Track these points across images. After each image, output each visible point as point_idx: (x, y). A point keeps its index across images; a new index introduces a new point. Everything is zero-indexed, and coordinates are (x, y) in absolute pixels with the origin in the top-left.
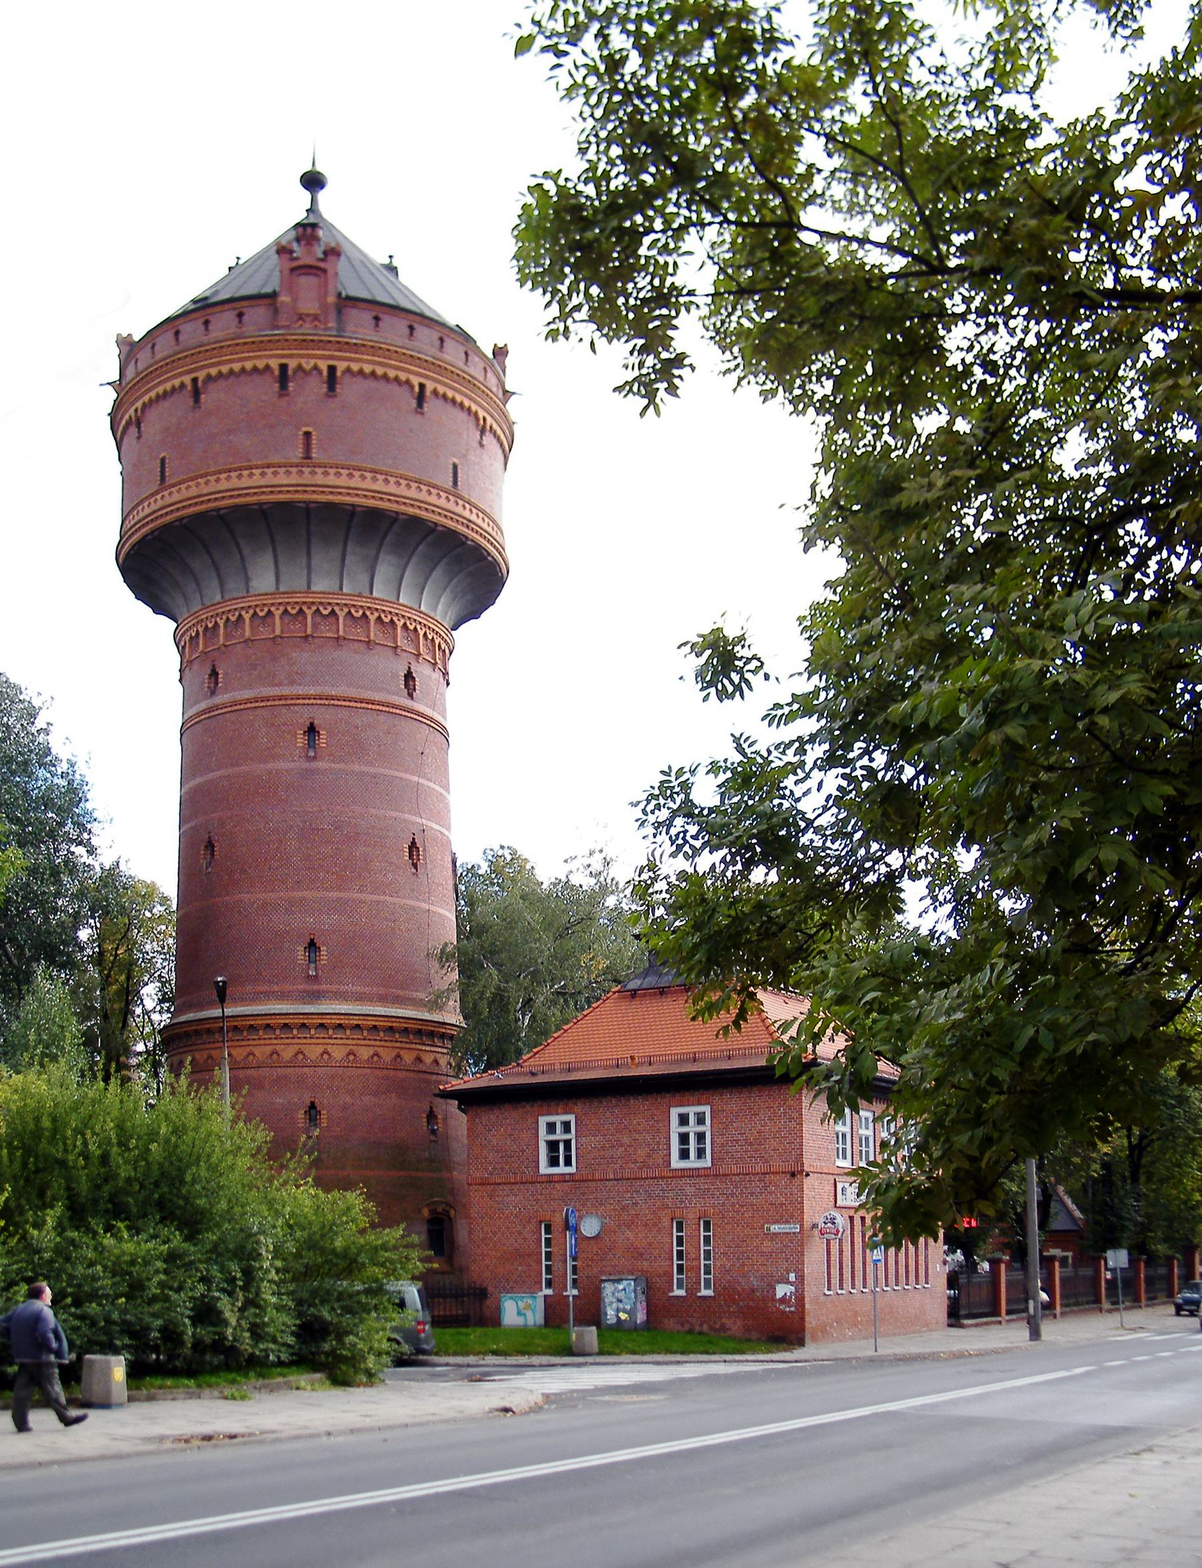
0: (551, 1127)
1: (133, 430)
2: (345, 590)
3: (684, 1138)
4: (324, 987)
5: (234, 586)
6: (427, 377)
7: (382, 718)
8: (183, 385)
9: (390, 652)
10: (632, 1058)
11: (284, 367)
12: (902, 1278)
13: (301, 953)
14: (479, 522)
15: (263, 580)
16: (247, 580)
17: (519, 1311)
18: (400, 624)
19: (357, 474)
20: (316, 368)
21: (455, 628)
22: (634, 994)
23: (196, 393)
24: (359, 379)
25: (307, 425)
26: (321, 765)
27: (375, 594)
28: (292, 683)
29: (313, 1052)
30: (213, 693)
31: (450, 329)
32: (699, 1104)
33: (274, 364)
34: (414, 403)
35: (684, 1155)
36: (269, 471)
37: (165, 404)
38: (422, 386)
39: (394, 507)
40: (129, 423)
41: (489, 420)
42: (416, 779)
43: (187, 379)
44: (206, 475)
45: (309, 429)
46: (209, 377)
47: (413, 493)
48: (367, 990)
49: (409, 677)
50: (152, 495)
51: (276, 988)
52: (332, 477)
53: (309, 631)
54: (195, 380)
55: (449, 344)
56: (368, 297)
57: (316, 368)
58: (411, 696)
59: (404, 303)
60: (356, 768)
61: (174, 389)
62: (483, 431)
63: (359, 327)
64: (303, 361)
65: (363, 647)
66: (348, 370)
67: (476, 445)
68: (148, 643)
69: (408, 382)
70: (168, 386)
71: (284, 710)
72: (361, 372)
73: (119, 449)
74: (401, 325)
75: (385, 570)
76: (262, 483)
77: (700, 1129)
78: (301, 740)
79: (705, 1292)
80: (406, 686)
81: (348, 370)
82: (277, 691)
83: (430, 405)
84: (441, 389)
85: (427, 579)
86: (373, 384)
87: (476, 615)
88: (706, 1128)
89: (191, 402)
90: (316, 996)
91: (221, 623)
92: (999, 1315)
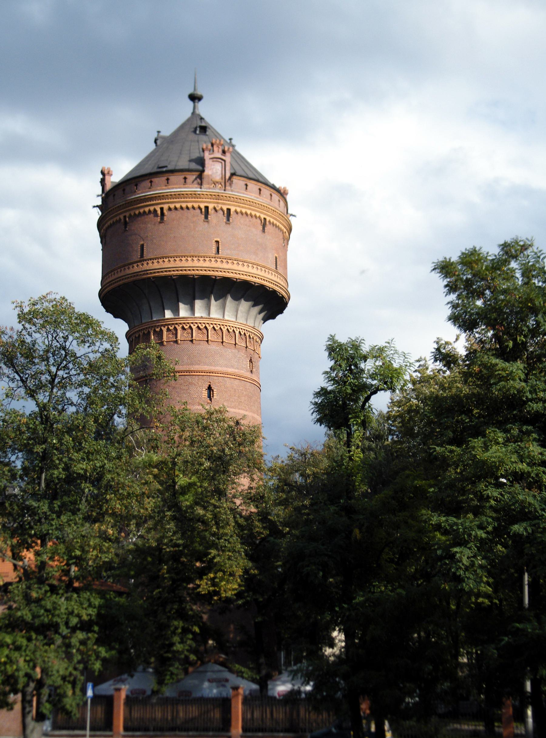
20: (222, 209)
25: (217, 237)
41: (268, 219)
43: (122, 217)
45: (218, 240)
54: (125, 217)
59: (261, 179)
61: (117, 221)
81: (236, 212)
84: (239, 210)
85: (237, 311)
87: (273, 317)
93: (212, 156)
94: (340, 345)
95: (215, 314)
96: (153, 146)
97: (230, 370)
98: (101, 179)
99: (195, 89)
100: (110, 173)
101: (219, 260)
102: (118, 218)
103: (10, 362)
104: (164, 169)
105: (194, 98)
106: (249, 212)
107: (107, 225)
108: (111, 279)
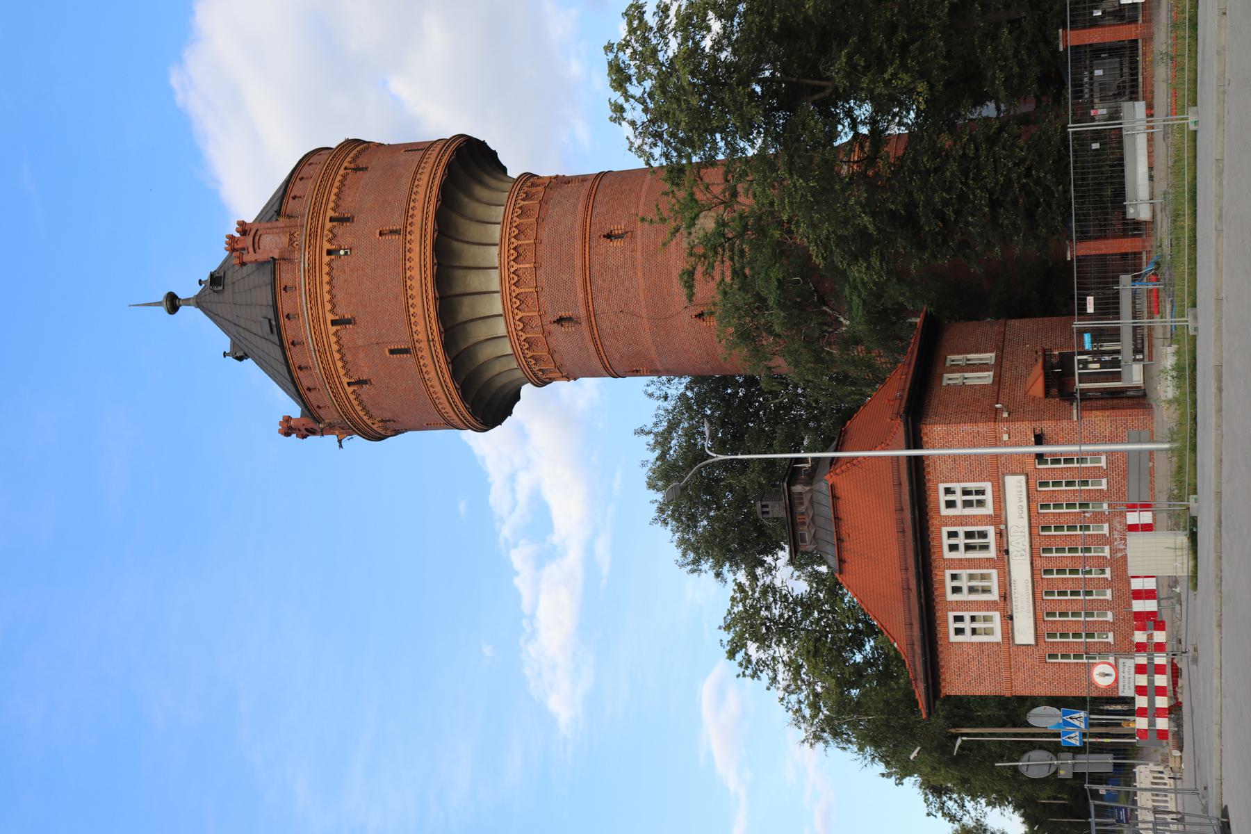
11: (334, 323)
19: (412, 310)
22: (841, 561)
23: (360, 382)
32: (937, 491)
43: (350, 390)
52: (419, 328)
57: (331, 231)
66: (332, 311)
73: (406, 430)
77: (962, 535)
81: (332, 311)
88: (957, 487)
93: (251, 249)
95: (500, 328)
96: (249, 362)
97: (579, 282)
99: (159, 304)
100: (288, 419)
101: (409, 228)
102: (352, 397)
104: (274, 323)
105: (173, 303)
108: (452, 413)
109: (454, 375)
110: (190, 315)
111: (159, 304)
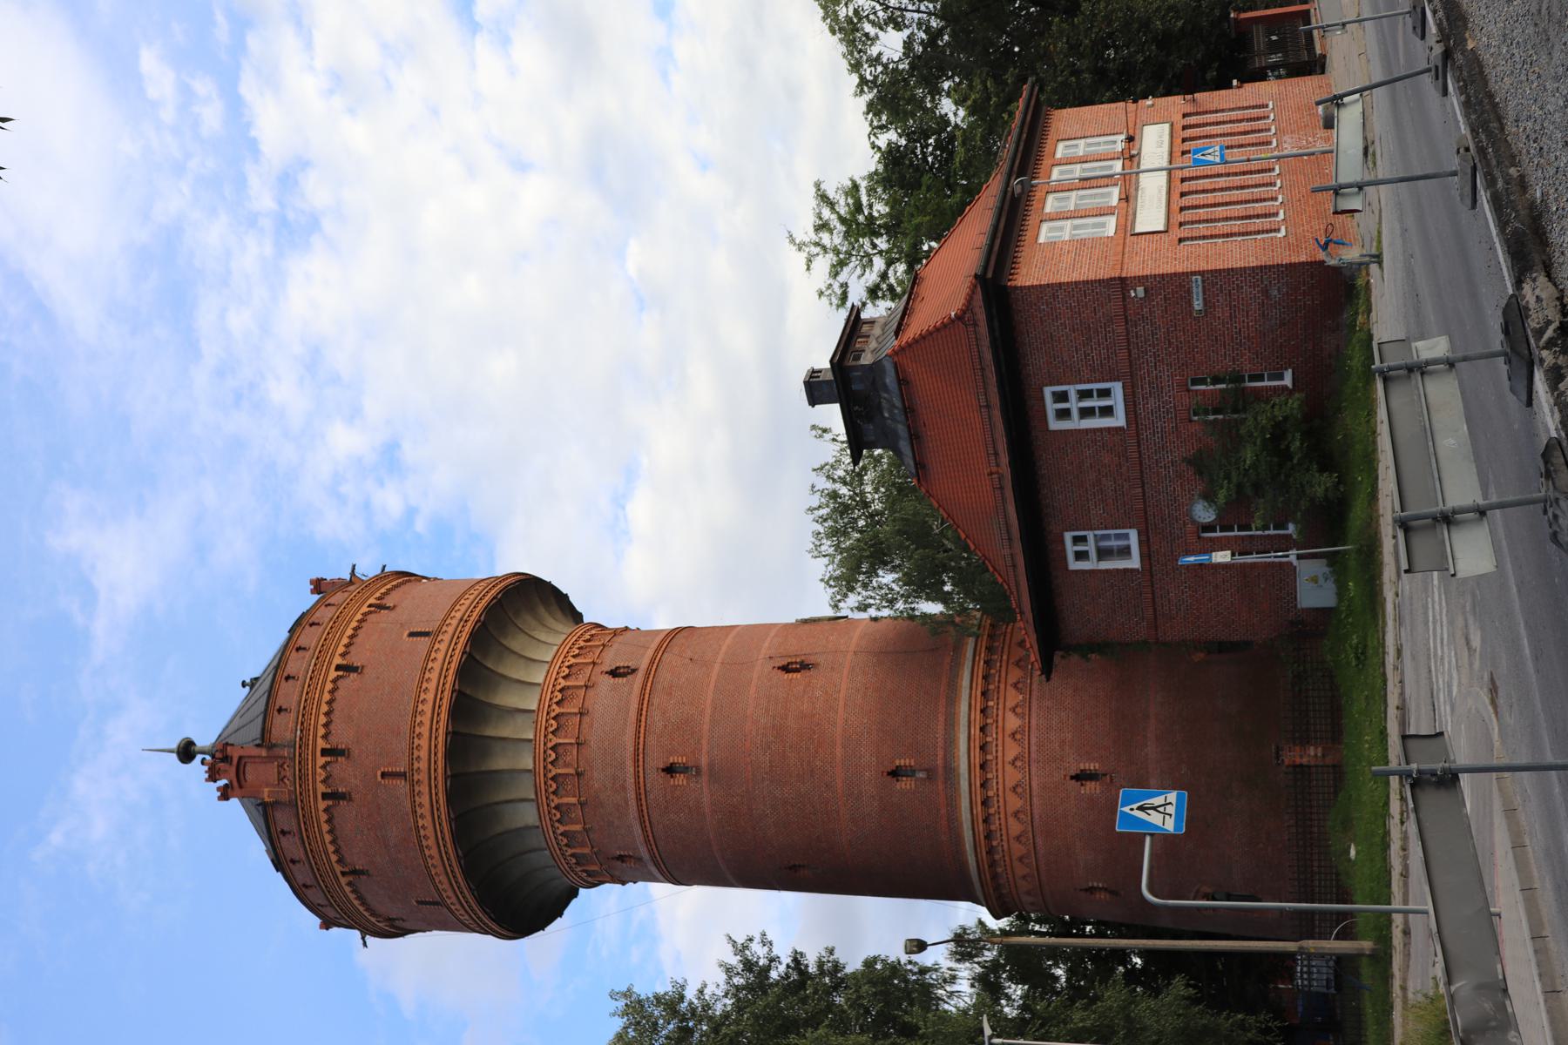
0: (1081, 556)
1: (397, 923)
2: (531, 736)
3: (1086, 413)
4: (940, 762)
5: (536, 840)
6: (330, 663)
7: (656, 701)
8: (349, 884)
9: (591, 693)
10: (991, 474)
12: (1260, 124)
13: (905, 784)
14: (463, 608)
15: (527, 815)
16: (527, 828)
17: (1314, 588)
18: (563, 683)
19: (417, 730)
20: (324, 767)
21: (577, 617)
23: (354, 872)
24: (332, 727)
26: (704, 761)
27: (534, 707)
28: (624, 788)
29: (1012, 776)
30: (640, 859)
31: (289, 639)
33: (322, 805)
34: (353, 676)
35: (1107, 411)
36: (419, 811)
37: (369, 898)
38: (338, 668)
39: (447, 694)
40: (392, 926)
41: (372, 601)
42: (717, 666)
43: (343, 881)
44: (427, 867)
46: (339, 861)
47: (434, 676)
48: (942, 719)
49: (614, 673)
50: (452, 912)
51: (943, 811)
53: (571, 771)
54: (343, 874)
55: (302, 642)
56: (260, 719)
58: (634, 671)
60: (706, 727)
62: (381, 607)
63: (284, 727)
64: (319, 779)
65: (586, 719)
66: (325, 737)
67: (392, 614)
68: (600, 908)
69: (334, 681)
70: (352, 896)
71: (651, 796)
72: (326, 725)
74: (285, 687)
75: (508, 698)
76: (429, 818)
78: (680, 779)
79: (1288, 381)
80: (624, 675)
81: (343, 655)
82: (633, 802)
83: (355, 659)
84: (341, 649)
86: (336, 716)
88: (1072, 390)
89: (363, 878)
90: (950, 771)
91: (570, 851)
92: (1388, 914)
94: (897, 170)
98: (580, 616)
99: (170, 751)
103: (791, 1026)
106: (354, 624)
107: (356, 903)
109: (457, 837)
110: (197, 768)
111: (170, 751)
